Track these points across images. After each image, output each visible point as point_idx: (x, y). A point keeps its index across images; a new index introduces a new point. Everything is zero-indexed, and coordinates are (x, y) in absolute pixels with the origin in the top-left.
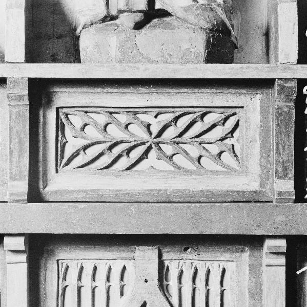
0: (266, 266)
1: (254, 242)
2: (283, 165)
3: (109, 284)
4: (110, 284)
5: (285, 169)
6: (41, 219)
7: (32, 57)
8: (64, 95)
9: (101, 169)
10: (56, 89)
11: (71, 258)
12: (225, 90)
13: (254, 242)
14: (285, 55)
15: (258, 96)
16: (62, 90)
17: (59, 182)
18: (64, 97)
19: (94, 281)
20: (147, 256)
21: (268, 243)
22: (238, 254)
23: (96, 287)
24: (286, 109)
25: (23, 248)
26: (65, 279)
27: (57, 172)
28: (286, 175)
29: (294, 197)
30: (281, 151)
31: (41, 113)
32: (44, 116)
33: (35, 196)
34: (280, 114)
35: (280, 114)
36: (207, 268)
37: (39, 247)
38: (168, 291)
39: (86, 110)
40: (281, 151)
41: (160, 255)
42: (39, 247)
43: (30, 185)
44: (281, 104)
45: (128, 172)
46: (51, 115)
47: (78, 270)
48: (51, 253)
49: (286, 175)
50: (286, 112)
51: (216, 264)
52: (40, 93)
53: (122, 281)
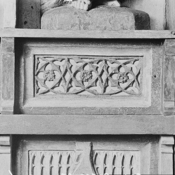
0: (162, 153)
1: (154, 138)
2: (7, 90)
3: (68, 165)
4: (106, 166)
5: (9, 93)
6: (21, 125)
7: (19, 25)
8: (33, 48)
9: (74, 94)
10: (29, 45)
11: (34, 150)
12: (135, 46)
13: (154, 138)
14: (7, 23)
15: (151, 51)
16: (32, 45)
17: (31, 103)
18: (35, 50)
19: (42, 164)
20: (84, 147)
21: (163, 139)
22: (72, 146)
23: (69, 167)
24: (9, 56)
25: (9, 144)
26: (33, 163)
27: (34, 96)
28: (9, 97)
29: (13, 111)
30: (6, 82)
31: (23, 60)
32: (25, 62)
33: (18, 110)
34: (5, 59)
35: (5, 59)
36: (51, 155)
37: (17, 142)
38: (97, 170)
39: (45, 56)
40: (6, 82)
41: (92, 147)
42: (17, 142)
43: (15, 103)
44: (5, 53)
45: (77, 96)
46: (30, 61)
47: (41, 157)
48: (24, 145)
49: (9, 97)
50: (9, 58)
51: (65, 153)
52: (21, 46)
53: (34, 164)
